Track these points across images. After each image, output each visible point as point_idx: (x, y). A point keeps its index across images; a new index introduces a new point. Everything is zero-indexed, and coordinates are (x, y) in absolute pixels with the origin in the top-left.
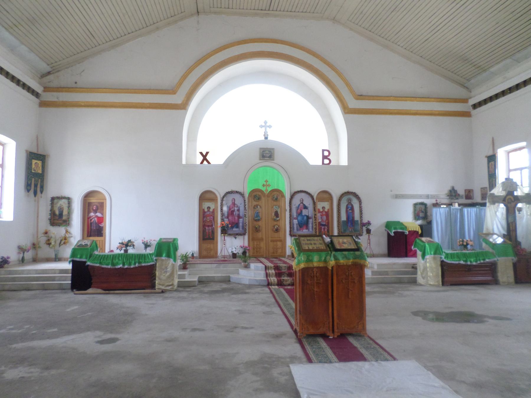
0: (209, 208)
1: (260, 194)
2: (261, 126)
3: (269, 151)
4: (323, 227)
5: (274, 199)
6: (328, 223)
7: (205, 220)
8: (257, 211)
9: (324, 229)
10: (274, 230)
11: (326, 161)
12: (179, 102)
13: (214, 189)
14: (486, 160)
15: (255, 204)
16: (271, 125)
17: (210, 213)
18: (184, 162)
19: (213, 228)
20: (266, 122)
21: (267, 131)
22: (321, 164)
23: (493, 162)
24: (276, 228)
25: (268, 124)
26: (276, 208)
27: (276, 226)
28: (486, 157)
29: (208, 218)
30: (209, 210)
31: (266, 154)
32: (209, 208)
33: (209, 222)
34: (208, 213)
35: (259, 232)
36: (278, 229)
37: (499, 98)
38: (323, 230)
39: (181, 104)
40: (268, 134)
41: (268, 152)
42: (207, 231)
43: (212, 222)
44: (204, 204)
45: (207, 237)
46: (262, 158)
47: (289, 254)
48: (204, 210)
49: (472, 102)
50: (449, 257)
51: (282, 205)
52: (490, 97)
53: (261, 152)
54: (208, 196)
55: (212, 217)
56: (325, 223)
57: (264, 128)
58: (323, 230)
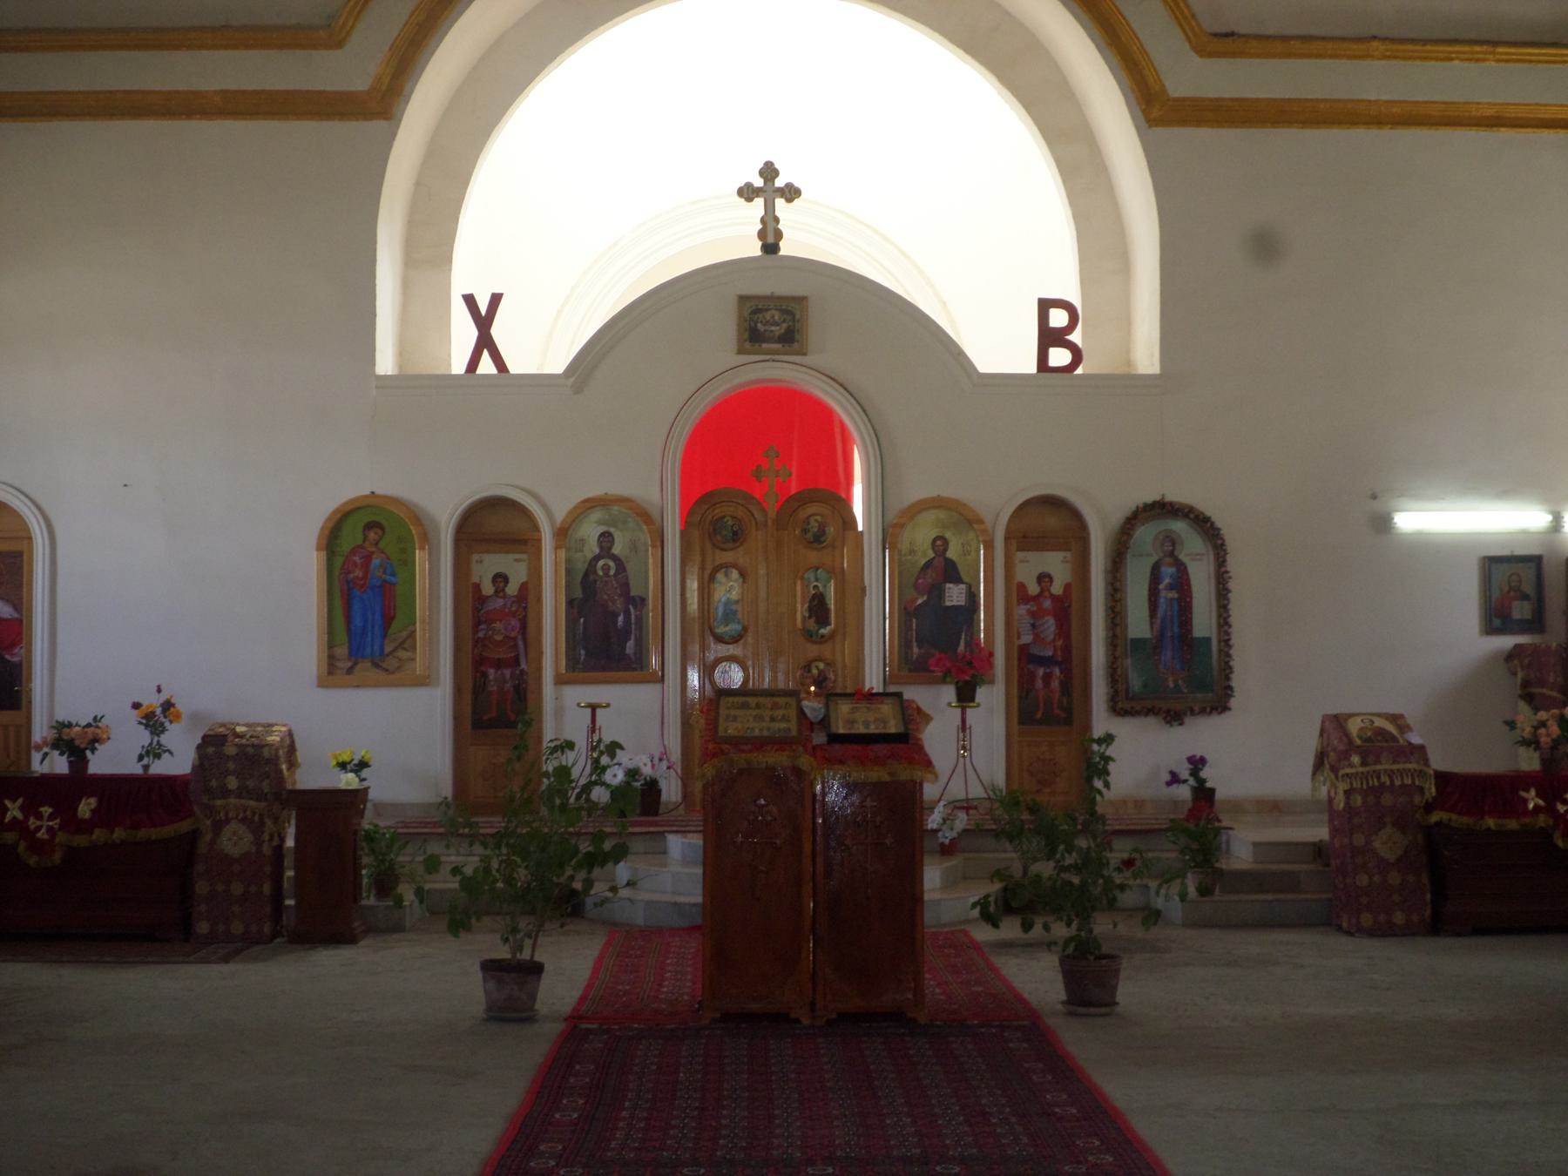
0: (501, 579)
4: (1041, 672)
5: (810, 536)
6: (1067, 649)
7: (481, 634)
9: (1047, 678)
11: (1058, 357)
12: (361, 84)
13: (523, 489)
18: (385, 363)
19: (522, 672)
20: (769, 171)
26: (817, 580)
27: (813, 665)
29: (498, 625)
30: (503, 590)
31: (766, 324)
32: (501, 579)
36: (825, 679)
38: (1039, 684)
42: (493, 687)
43: (516, 646)
46: (748, 345)
53: (746, 314)
55: (514, 622)
56: (1050, 653)
58: (1039, 684)
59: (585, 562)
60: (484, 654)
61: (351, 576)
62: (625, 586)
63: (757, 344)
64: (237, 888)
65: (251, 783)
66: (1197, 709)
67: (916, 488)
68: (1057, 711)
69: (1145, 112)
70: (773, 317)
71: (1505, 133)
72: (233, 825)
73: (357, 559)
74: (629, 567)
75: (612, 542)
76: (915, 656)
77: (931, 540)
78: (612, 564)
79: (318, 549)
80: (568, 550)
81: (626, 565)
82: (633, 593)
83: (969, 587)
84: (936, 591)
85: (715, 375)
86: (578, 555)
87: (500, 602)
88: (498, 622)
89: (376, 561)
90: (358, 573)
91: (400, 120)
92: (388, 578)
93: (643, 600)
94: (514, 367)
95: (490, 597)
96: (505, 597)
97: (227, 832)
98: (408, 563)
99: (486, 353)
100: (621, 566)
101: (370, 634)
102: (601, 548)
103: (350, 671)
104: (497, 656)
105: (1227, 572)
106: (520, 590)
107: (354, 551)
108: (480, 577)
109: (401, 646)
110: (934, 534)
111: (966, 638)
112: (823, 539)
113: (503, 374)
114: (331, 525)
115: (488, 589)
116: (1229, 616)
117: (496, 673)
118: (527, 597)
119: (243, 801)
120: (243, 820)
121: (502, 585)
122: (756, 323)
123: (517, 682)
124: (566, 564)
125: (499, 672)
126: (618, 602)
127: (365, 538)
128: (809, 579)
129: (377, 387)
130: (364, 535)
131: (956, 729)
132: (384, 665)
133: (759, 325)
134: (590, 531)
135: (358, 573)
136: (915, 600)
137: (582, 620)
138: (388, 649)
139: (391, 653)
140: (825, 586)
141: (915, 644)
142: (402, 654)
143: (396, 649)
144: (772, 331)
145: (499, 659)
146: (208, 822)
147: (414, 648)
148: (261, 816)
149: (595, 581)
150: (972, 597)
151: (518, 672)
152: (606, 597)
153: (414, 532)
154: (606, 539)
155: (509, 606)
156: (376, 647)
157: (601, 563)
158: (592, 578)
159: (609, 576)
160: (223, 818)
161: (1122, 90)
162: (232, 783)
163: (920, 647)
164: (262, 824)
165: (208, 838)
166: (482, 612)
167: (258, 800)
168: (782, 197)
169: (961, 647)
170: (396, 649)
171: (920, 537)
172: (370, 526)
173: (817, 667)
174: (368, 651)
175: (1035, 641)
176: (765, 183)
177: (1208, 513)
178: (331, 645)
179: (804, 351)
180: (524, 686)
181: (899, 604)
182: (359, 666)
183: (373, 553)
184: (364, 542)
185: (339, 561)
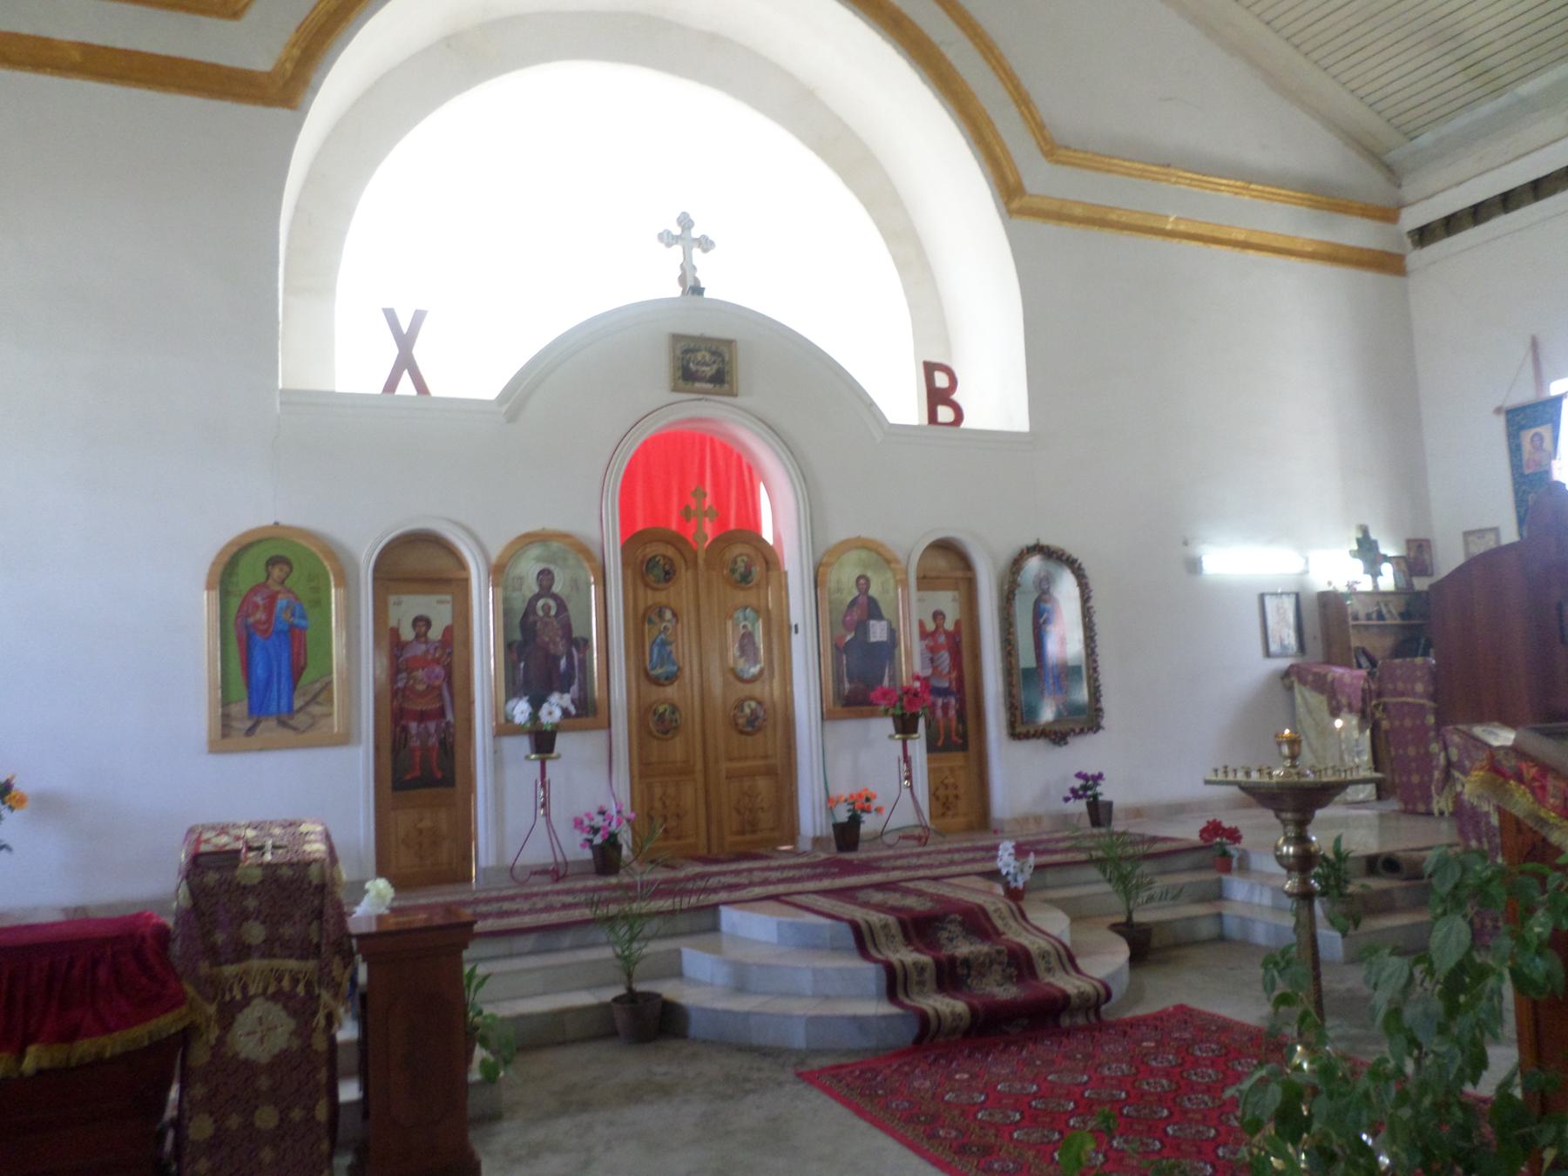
0: (422, 623)
1: (670, 552)
2: (667, 239)
3: (713, 353)
4: (940, 702)
5: (737, 576)
6: (960, 680)
7: (400, 684)
8: (663, 636)
9: (945, 707)
10: (741, 721)
11: (945, 414)
12: (262, 62)
13: (456, 523)
14: (1500, 423)
15: (650, 603)
16: (711, 238)
17: (427, 651)
18: (280, 386)
19: (448, 724)
20: (685, 222)
21: (695, 262)
22: (925, 420)
23: (1549, 426)
24: (747, 711)
25: (696, 233)
26: (745, 619)
27: (746, 704)
28: (1498, 411)
29: (420, 674)
30: (425, 634)
31: (698, 364)
32: (422, 623)
33: (422, 695)
34: (420, 649)
35: (672, 738)
36: (757, 718)
37: (1517, 207)
38: (939, 713)
39: (269, 74)
40: (697, 275)
41: (708, 357)
42: (415, 743)
43: (440, 695)
44: (399, 603)
45: (418, 773)
46: (681, 382)
47: (818, 834)
48: (395, 632)
49: (1413, 218)
50: (639, 858)
51: (770, 605)
52: (1471, 207)
53: (678, 352)
54: (414, 561)
55: (438, 670)
56: (946, 684)
57: (677, 250)
58: (939, 713)
59: (524, 601)
60: (406, 705)
61: (251, 620)
62: (567, 628)
63: (690, 384)
64: (267, 1118)
65: (287, 931)
66: (1077, 730)
67: (840, 530)
68: (955, 738)
69: (1007, 204)
70: (704, 357)
71: (1251, 253)
72: (258, 1008)
73: (259, 599)
74: (570, 606)
75: (552, 580)
76: (847, 691)
77: (855, 579)
78: (552, 603)
79: (209, 587)
80: (505, 589)
81: (567, 603)
82: (575, 634)
83: (890, 623)
84: (861, 628)
85: (651, 410)
86: (515, 594)
87: (423, 647)
88: (420, 671)
89: (281, 602)
90: (260, 615)
91: (306, 113)
92: (296, 621)
93: (586, 642)
94: (437, 389)
95: (411, 642)
96: (426, 642)
97: (247, 1019)
98: (322, 603)
99: (406, 374)
100: (562, 607)
101: (275, 687)
102: (540, 585)
103: (250, 732)
104: (419, 708)
105: (1092, 607)
106: (444, 635)
107: (254, 590)
108: (399, 620)
109: (314, 699)
110: (857, 573)
111: (889, 672)
112: (750, 579)
113: (424, 397)
114: (226, 559)
115: (407, 634)
116: (1096, 646)
117: (418, 726)
118: (455, 642)
119: (276, 963)
120: (274, 997)
121: (423, 629)
122: (688, 363)
123: (443, 735)
124: (504, 603)
125: (423, 726)
126: (560, 644)
127: (268, 576)
128: (738, 618)
129: (281, 403)
130: (267, 570)
131: (897, 760)
132: (292, 722)
133: (691, 365)
134: (528, 568)
135: (260, 615)
136: (844, 637)
137: (522, 665)
138: (298, 704)
139: (301, 709)
140: (753, 625)
141: (846, 679)
142: (316, 709)
143: (307, 704)
144: (704, 371)
145: (421, 711)
146: (212, 1009)
147: (331, 701)
148: (309, 985)
149: (535, 623)
150: (893, 633)
151: (443, 724)
152: (547, 639)
153: (328, 568)
154: (545, 576)
155: (432, 651)
156: (284, 702)
157: (540, 603)
158: (531, 619)
159: (550, 617)
160: (239, 997)
161: (990, 184)
162: (255, 932)
163: (850, 682)
164: (312, 997)
165: (214, 1034)
166: (401, 659)
167: (303, 957)
168: (699, 247)
169: (886, 683)
170: (307, 704)
171: (845, 576)
172: (273, 561)
173: (749, 706)
174: (273, 708)
175: (933, 674)
176: (683, 231)
177: (1075, 556)
178: (226, 702)
179: (735, 391)
180: (451, 739)
181: (832, 641)
182: (262, 726)
183: (278, 593)
184: (268, 578)
185: (235, 603)
